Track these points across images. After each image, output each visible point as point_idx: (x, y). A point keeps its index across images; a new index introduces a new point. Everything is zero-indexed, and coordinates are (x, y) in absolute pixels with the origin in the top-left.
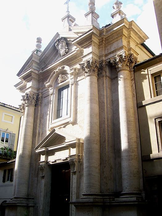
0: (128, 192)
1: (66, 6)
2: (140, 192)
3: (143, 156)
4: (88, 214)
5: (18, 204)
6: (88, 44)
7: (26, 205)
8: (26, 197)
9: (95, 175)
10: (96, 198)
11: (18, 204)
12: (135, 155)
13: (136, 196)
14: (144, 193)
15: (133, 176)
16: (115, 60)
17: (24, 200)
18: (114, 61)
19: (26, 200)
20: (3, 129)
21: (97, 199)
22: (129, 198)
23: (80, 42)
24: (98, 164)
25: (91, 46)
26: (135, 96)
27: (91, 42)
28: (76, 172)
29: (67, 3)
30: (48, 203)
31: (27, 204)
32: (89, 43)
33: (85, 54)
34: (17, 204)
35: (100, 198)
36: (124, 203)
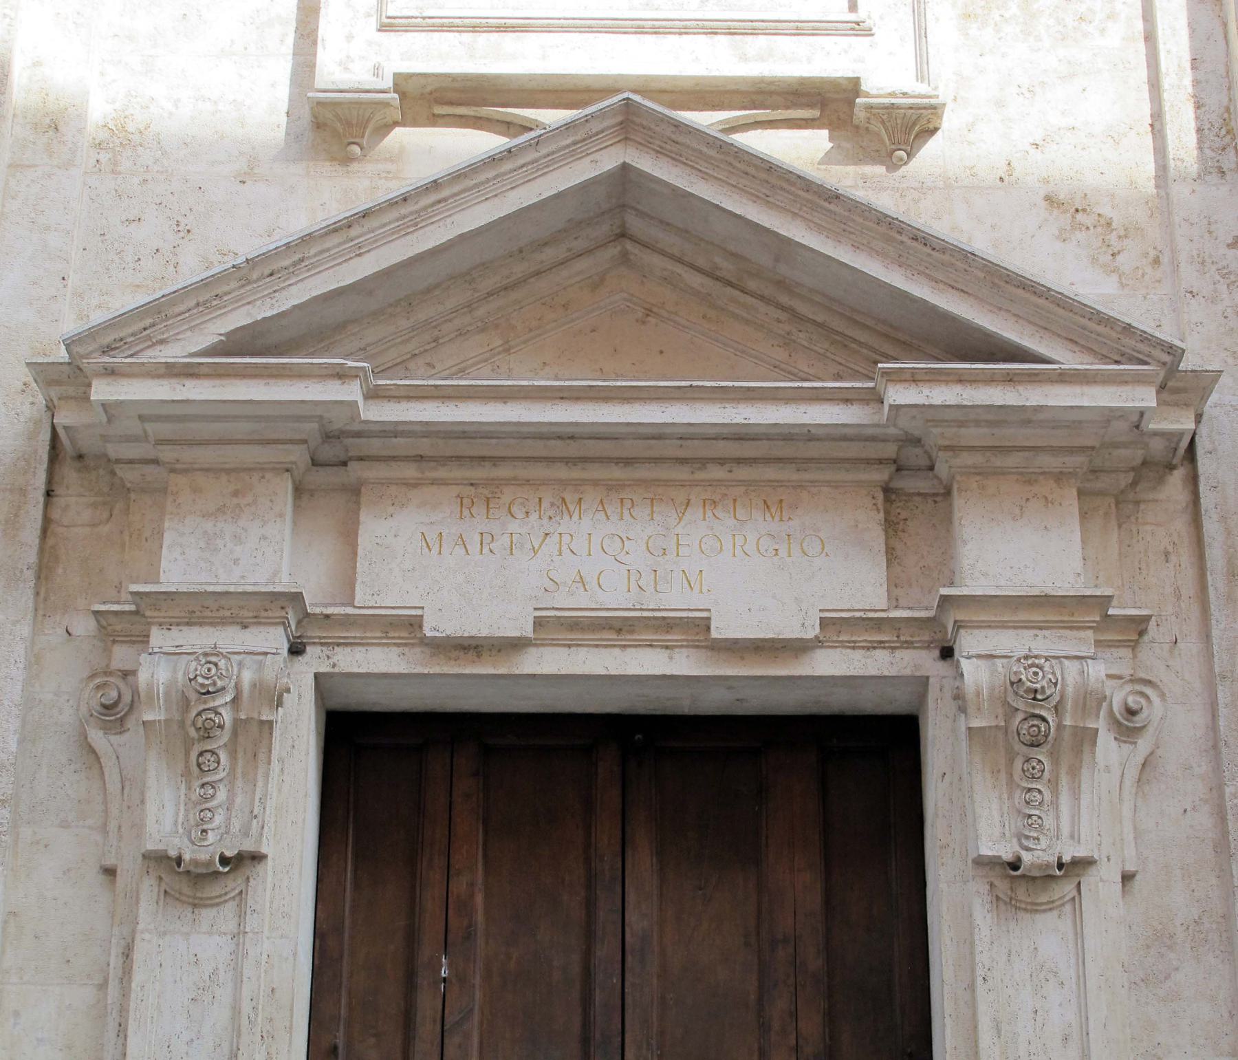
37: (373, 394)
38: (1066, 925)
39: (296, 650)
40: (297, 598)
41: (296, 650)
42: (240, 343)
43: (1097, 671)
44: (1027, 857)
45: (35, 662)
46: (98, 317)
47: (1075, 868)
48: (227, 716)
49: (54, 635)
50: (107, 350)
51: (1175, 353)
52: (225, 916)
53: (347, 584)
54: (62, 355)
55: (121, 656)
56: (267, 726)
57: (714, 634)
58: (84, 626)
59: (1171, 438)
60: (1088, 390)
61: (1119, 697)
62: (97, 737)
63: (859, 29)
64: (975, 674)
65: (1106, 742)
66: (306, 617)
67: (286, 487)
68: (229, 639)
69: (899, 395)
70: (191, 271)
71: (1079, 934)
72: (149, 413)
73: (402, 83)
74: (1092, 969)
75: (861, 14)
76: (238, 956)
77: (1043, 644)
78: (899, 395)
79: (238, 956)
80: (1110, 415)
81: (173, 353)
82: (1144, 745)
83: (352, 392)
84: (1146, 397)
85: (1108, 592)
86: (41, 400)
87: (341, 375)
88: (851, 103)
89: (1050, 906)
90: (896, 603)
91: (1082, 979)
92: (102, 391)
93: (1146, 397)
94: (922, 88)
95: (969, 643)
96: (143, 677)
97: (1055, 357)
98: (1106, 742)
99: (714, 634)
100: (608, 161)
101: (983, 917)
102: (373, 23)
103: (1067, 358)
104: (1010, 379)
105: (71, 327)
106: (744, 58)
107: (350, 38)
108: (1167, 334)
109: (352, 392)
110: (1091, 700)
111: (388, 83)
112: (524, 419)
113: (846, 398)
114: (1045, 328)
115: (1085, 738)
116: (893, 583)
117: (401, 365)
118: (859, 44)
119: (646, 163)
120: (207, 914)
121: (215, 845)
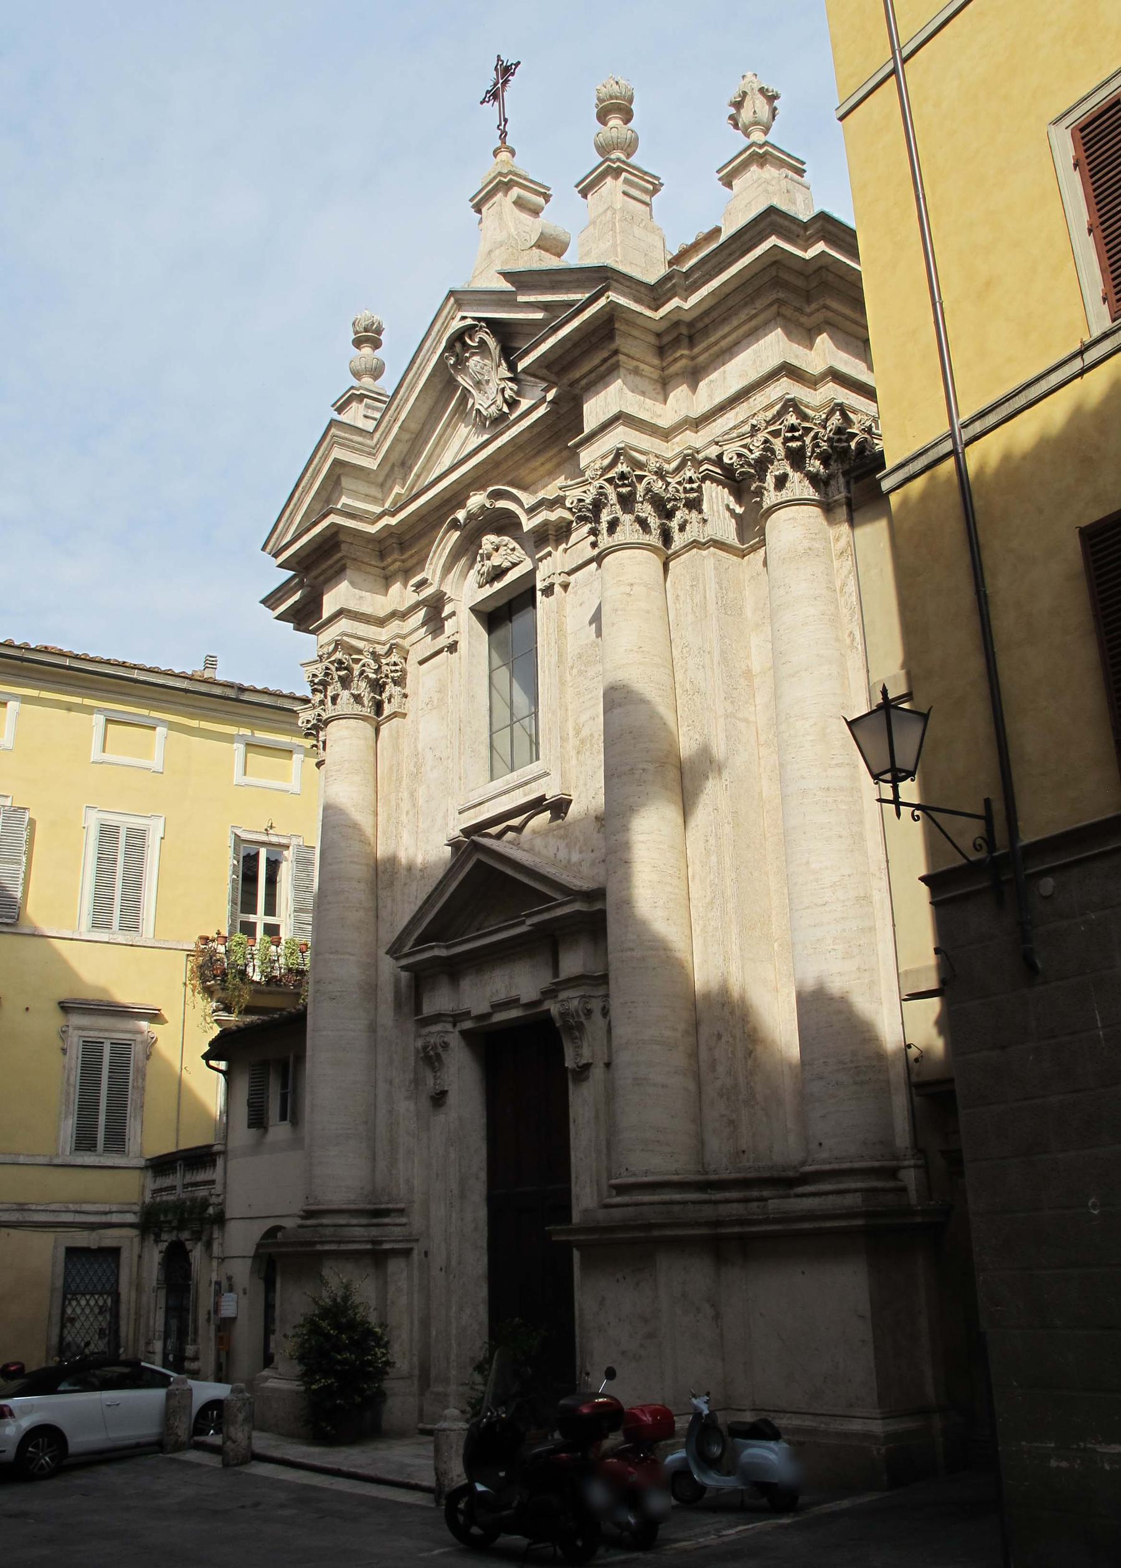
0: (827, 1167)
1: (492, 108)
2: (894, 1163)
3: (906, 973)
4: (637, 1284)
5: (327, 1247)
6: (603, 368)
7: (369, 1246)
8: (361, 1206)
9: (664, 1086)
10: (672, 1203)
11: (322, 1243)
12: (859, 969)
13: (859, 1185)
14: (915, 1166)
15: (856, 1083)
16: (744, 446)
17: (354, 1221)
18: (739, 455)
19: (364, 1221)
20: (335, 722)
21: (756, 1204)
22: (831, 1197)
23: (560, 357)
24: (682, 1026)
25: (615, 374)
26: (860, 648)
27: (616, 352)
28: (587, 1067)
29: (495, 95)
30: (476, 1229)
31: (373, 1242)
32: (605, 360)
33: (589, 425)
34: (319, 1247)
35: (693, 1202)
36: (806, 1226)
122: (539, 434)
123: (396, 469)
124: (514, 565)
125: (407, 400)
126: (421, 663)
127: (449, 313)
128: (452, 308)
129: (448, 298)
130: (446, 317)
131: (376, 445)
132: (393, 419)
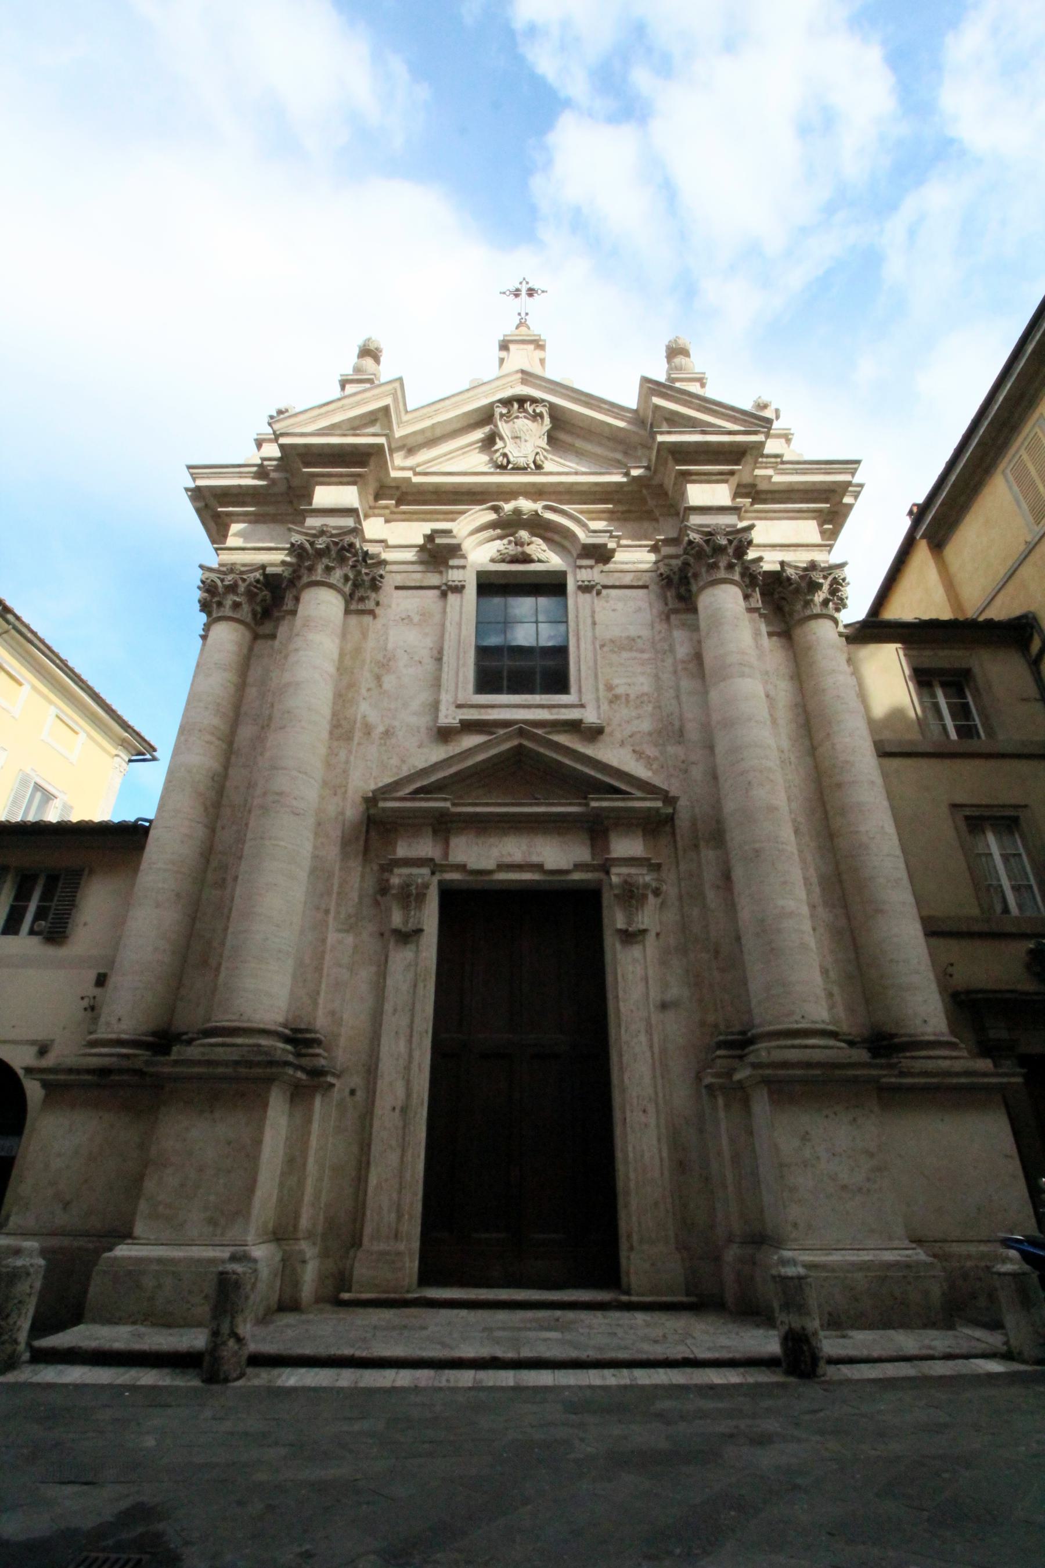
37: (454, 805)
38: (641, 947)
39: (433, 873)
40: (432, 860)
41: (433, 873)
42: (417, 791)
43: (648, 878)
44: (630, 929)
45: (363, 876)
46: (380, 785)
47: (644, 932)
48: (414, 891)
49: (368, 870)
50: (383, 793)
51: (667, 792)
52: (412, 947)
53: (446, 855)
54: (371, 795)
55: (386, 875)
56: (425, 895)
57: (383, 518)
58: (376, 867)
59: (667, 815)
60: (646, 802)
61: (654, 884)
62: (379, 897)
63: (582, 706)
64: (615, 879)
65: (651, 897)
66: (435, 865)
67: (430, 829)
68: (415, 871)
69: (594, 804)
70: (405, 772)
71: (645, 951)
72: (393, 809)
73: (461, 721)
74: (648, 959)
75: (583, 702)
76: (417, 957)
77: (633, 871)
78: (594, 804)
79: (417, 957)
80: (650, 809)
81: (401, 794)
82: (662, 896)
83: (448, 804)
84: (659, 804)
85: (650, 856)
86: (365, 806)
87: (445, 800)
88: (580, 726)
89: (636, 943)
90: (593, 859)
91: (645, 961)
92: (381, 804)
93: (659, 804)
94: (599, 721)
95: (614, 870)
96: (392, 881)
97: (633, 792)
98: (651, 897)
99: (383, 518)
100: (515, 742)
101: (618, 946)
102: (454, 706)
103: (639, 794)
104: (623, 799)
105: (373, 787)
106: (552, 714)
107: (447, 710)
108: (665, 787)
109: (448, 804)
110: (646, 886)
111: (458, 721)
112: (86, 725)
113: (580, 804)
114: (632, 785)
115: (644, 897)
116: (593, 855)
117: (461, 797)
118: (582, 710)
119: (526, 743)
120: (409, 946)
121: (411, 926)
122: (595, 493)
123: (406, 449)
124: (540, 561)
125: (447, 411)
126: (397, 588)
127: (512, 381)
128: (515, 380)
129: (517, 372)
130: (508, 383)
131: (405, 422)
132: (428, 415)
